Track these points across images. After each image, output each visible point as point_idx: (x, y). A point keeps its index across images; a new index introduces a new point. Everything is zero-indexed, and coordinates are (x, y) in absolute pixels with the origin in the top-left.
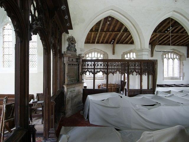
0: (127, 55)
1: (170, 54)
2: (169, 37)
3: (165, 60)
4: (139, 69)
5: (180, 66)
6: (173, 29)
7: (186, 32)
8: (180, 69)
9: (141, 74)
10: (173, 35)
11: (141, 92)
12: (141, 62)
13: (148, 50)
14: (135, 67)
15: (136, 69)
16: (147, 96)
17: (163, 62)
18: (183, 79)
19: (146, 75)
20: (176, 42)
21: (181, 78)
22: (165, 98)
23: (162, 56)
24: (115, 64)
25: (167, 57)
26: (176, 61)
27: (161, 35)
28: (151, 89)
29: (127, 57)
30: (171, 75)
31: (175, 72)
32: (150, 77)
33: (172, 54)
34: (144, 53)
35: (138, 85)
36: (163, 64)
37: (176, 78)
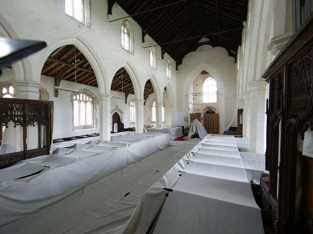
0: (8, 89)
1: (81, 95)
2: (73, 70)
3: (76, 103)
4: (20, 116)
5: (93, 111)
6: (81, 62)
7: (92, 70)
8: (93, 115)
9: (24, 125)
10: (83, 71)
11: (26, 154)
12: (24, 104)
13: (38, 84)
14: (11, 112)
15: (15, 116)
16: (34, 160)
17: (73, 105)
18: (96, 127)
19: (34, 126)
20: (89, 80)
21: (95, 125)
22: (66, 156)
23: (72, 97)
24: (18, 107)
25: (78, 99)
26: (89, 105)
27: (67, 66)
28: (44, 146)
29: (8, 93)
30: (83, 123)
31: (88, 119)
32: (43, 127)
33: (84, 96)
34: (30, 89)
35: (21, 144)
36: (73, 108)
37: (89, 127)
